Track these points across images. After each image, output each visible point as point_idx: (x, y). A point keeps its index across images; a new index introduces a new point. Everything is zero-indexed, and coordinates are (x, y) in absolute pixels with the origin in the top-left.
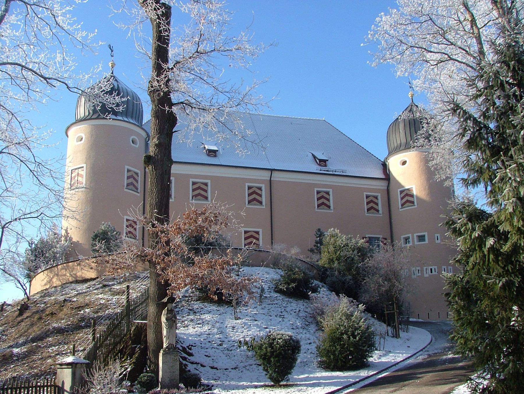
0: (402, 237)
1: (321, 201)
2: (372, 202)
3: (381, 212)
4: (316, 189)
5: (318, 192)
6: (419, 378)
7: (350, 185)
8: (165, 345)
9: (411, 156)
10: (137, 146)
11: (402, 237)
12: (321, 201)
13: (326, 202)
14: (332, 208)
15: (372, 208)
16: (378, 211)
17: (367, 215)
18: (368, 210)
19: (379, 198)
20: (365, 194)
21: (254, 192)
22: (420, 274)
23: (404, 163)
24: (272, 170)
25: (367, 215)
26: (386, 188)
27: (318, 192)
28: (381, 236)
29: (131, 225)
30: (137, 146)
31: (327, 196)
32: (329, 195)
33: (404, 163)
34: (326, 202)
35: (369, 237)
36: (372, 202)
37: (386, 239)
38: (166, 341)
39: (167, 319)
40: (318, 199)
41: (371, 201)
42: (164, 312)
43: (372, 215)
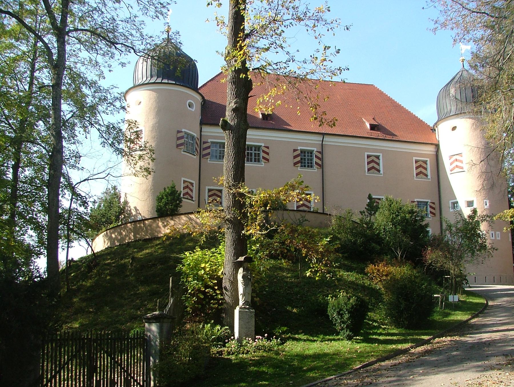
0: (451, 201)
1: (371, 165)
2: (421, 166)
3: (429, 177)
4: (366, 154)
5: (368, 157)
6: (418, 380)
7: (356, 146)
8: (241, 302)
9: (465, 124)
10: (193, 110)
11: (451, 201)
12: (371, 165)
13: (376, 166)
14: (382, 172)
15: (421, 172)
16: (427, 176)
17: (415, 179)
18: (369, 170)
19: (428, 163)
20: (414, 158)
21: (373, 161)
22: (494, 238)
23: (454, 128)
24: (323, 134)
25: (415, 179)
26: (435, 153)
27: (368, 157)
28: (430, 201)
29: (187, 187)
30: (193, 110)
31: (424, 165)
32: (379, 159)
33: (454, 128)
34: (376, 166)
35: (418, 202)
36: (421, 166)
37: (434, 203)
38: (242, 299)
39: (243, 277)
40: (369, 163)
41: (373, 161)
42: (241, 270)
43: (421, 179)
